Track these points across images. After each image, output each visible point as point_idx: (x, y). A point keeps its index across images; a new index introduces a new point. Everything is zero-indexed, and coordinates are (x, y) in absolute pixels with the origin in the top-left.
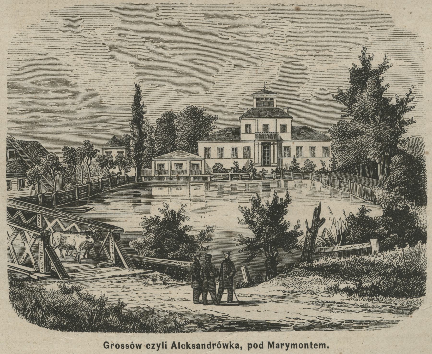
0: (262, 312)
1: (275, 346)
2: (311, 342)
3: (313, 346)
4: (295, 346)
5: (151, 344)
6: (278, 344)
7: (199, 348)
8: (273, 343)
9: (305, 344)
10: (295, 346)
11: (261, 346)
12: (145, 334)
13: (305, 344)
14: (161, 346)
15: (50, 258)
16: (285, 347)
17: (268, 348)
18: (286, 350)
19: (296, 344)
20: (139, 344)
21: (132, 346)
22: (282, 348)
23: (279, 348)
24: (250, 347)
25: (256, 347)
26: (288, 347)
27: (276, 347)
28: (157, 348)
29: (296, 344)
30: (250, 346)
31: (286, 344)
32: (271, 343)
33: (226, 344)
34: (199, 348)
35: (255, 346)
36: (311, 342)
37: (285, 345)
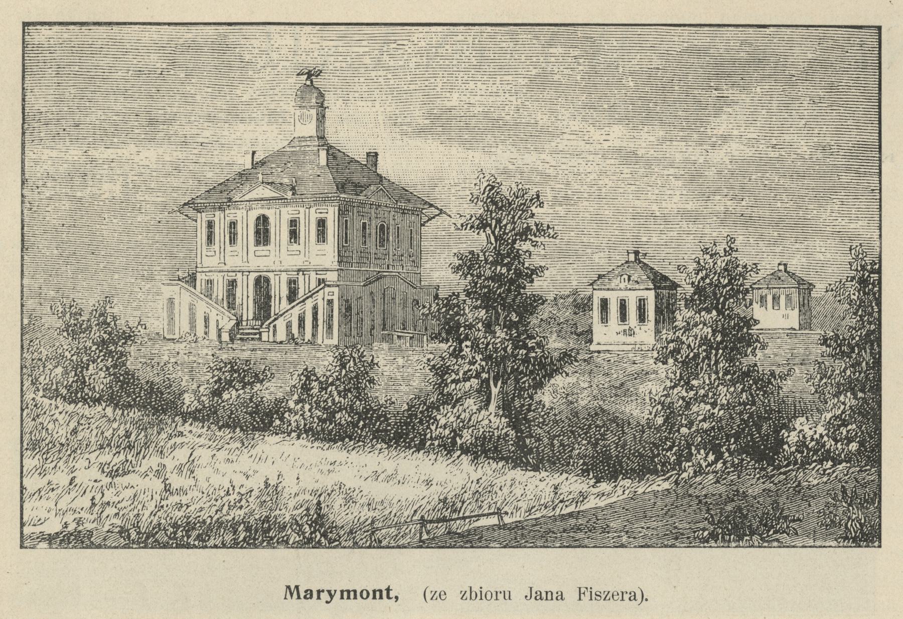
8: (297, 587)
13: (374, 591)
16: (325, 596)
19: (355, 591)
26: (332, 597)
29: (355, 591)
32: (292, 588)
35: (365, 595)
37: (326, 593)
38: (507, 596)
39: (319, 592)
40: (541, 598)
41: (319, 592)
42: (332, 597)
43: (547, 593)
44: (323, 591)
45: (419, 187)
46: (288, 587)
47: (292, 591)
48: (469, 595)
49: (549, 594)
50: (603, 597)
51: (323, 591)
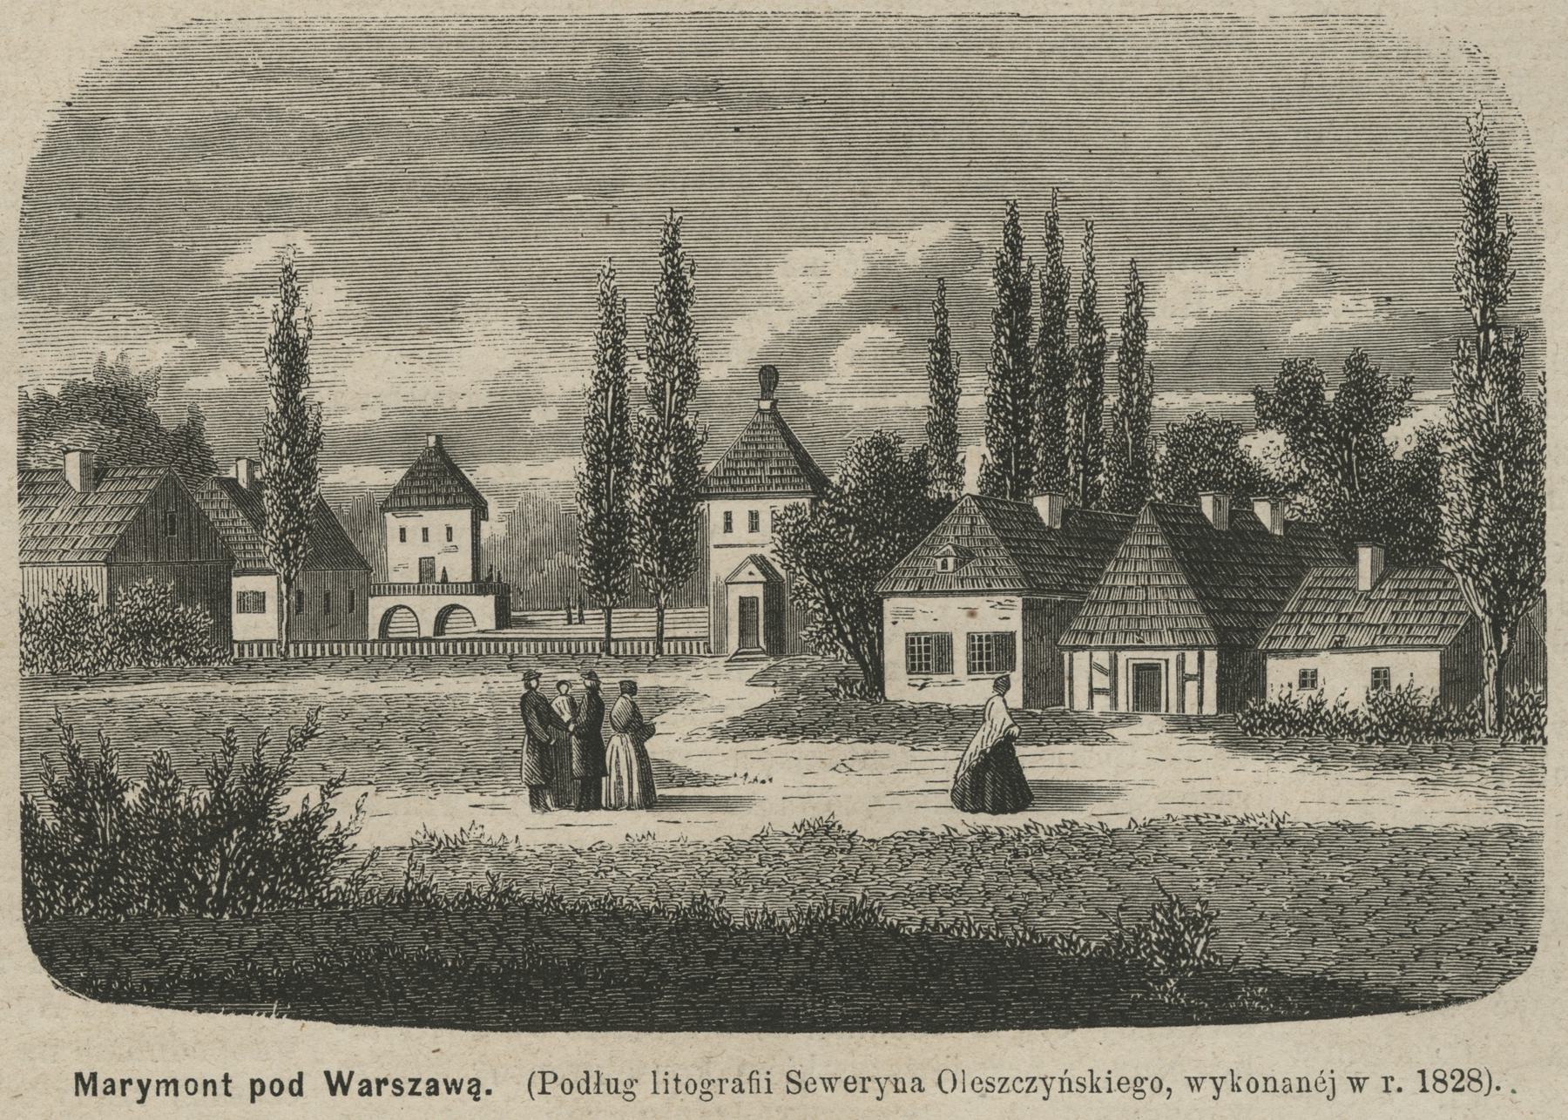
0: (1169, 760)
1: (100, 1087)
2: (226, 1075)
3: (681, 1087)
4: (172, 1087)
5: (405, 1081)
6: (368, 1081)
7: (369, 1093)
8: (94, 1076)
9: (206, 1083)
10: (172, 1087)
11: (296, 1087)
12: (1055, 1035)
13: (206, 1083)
14: (1227, 1085)
15: (761, 623)
16: (134, 1092)
17: (77, 1094)
18: (141, 1101)
19: (175, 1082)
20: (454, 1082)
21: (590, 1084)
22: (379, 1093)
23: (113, 1092)
24: (258, 1089)
25: (276, 1090)
26: (144, 1091)
27: (105, 1092)
28: (1042, 1092)
29: (175, 1082)
30: (337, 1084)
31: (140, 1082)
32: (86, 1078)
33: (454, 1082)
34: (369, 1093)
35: (276, 1089)
36: (226, 1075)
37: (135, 1084)
38: (297, 1087)
39: (123, 1082)
40: (742, 1091)
41: (123, 1082)
42: (144, 1091)
43: (588, 1091)
44: (385, 1081)
45: (794, 331)
46: (79, 1076)
47: (85, 1083)
48: (337, 1084)
49: (1271, 1083)
50: (998, 1086)
51: (130, 1081)
